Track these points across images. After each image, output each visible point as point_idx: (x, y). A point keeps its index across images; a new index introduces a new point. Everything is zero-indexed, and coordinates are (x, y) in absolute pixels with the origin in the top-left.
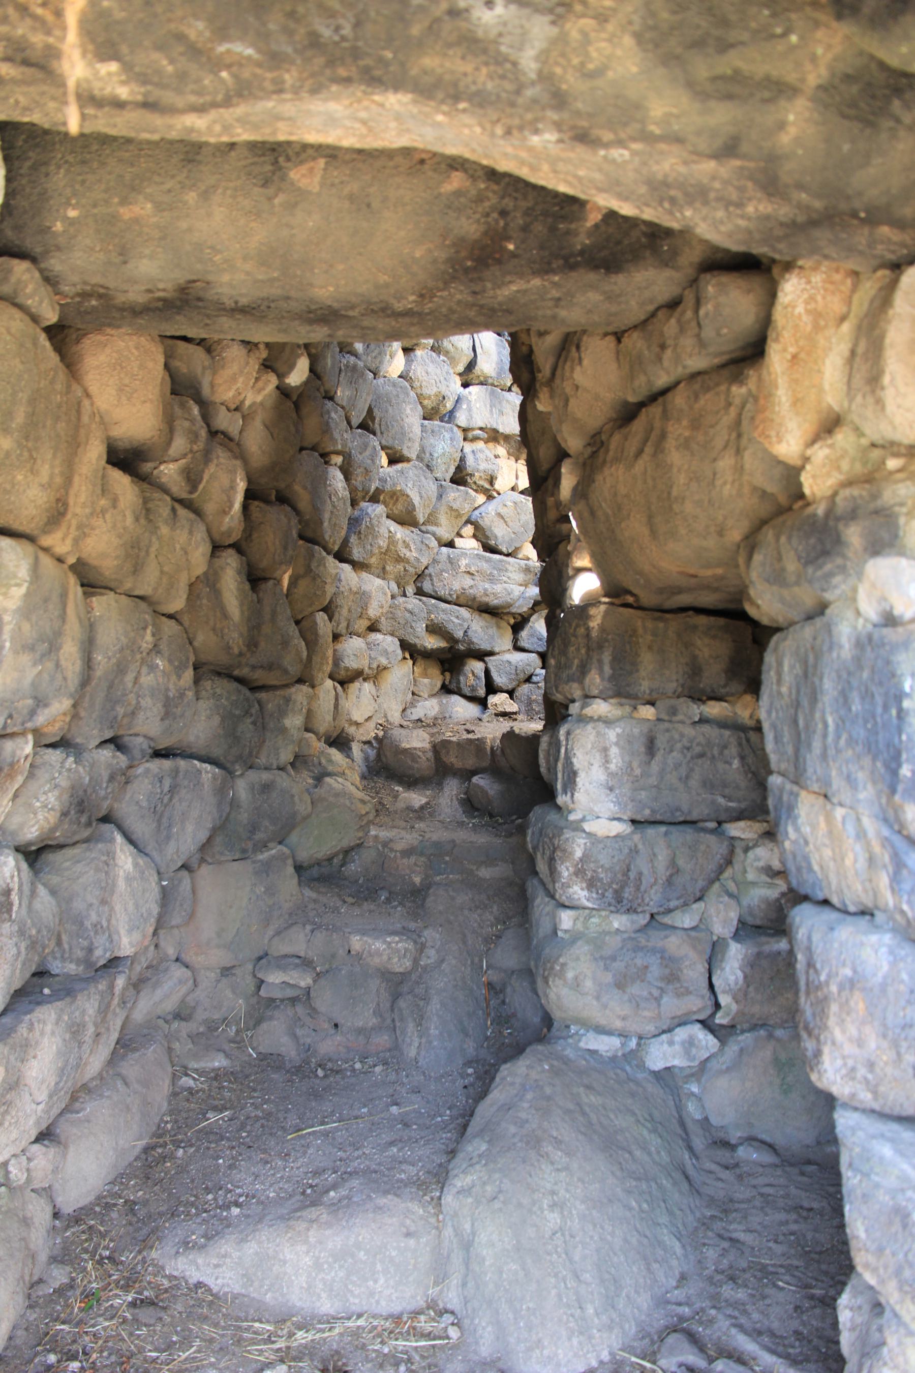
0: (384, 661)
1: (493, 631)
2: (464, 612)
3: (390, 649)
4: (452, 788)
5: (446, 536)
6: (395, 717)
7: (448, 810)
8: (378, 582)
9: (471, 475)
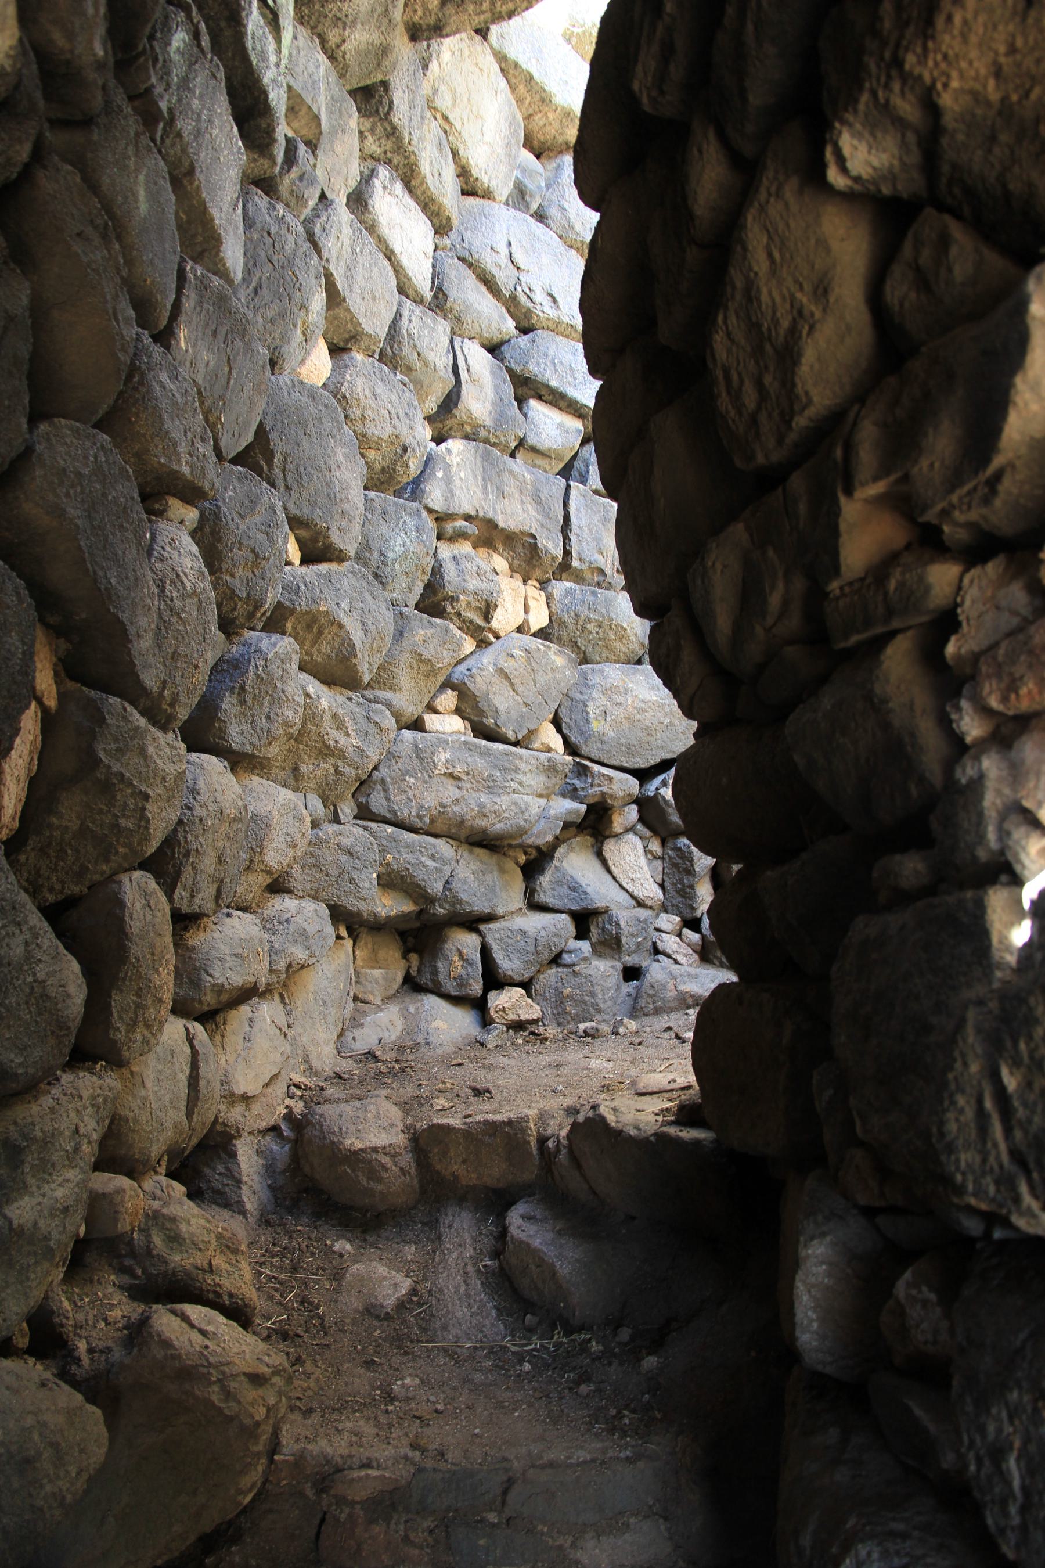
0: (300, 954)
1: (493, 878)
2: (444, 847)
3: (312, 929)
4: (462, 1237)
5: (411, 710)
6: (325, 1058)
7: (461, 1312)
8: (285, 795)
9: (453, 600)
